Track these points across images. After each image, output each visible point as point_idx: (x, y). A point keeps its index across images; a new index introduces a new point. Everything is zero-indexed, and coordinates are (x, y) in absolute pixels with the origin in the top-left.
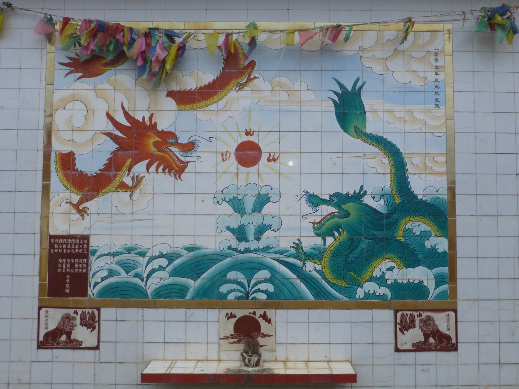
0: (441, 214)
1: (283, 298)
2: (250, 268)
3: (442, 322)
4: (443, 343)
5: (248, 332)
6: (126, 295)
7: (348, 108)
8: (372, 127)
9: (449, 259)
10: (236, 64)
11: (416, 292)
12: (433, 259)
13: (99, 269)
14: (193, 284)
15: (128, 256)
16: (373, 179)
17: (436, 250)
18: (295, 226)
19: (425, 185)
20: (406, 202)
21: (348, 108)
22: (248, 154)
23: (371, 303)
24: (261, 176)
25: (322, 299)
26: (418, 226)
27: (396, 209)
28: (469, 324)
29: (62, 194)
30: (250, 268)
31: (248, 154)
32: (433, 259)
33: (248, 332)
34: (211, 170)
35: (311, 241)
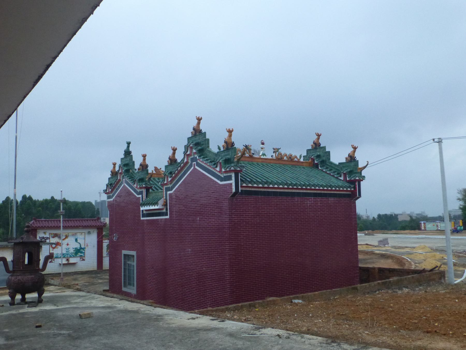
0: (83, 249)
1: (71, 257)
2: (68, 254)
3: (84, 258)
4: (84, 260)
5: (68, 260)
6: (57, 258)
7: (76, 240)
8: (78, 242)
9: (84, 253)
10: (67, 237)
11: (254, 177)
12: (83, 253)
13: (55, 256)
14: (64, 256)
15: (57, 254)
16: (78, 246)
17: (397, 219)
18: (72, 251)
19: (83, 247)
20: (81, 248)
21: (76, 240)
22: (68, 244)
23: (78, 257)
24: (69, 246)
25: (74, 257)
26: (82, 250)
27: (383, 308)
28: (86, 258)
29: (51, 249)
30: (68, 254)
31: (68, 244)
32: (83, 253)
33: (68, 260)
34: (64, 246)
35: (73, 252)
